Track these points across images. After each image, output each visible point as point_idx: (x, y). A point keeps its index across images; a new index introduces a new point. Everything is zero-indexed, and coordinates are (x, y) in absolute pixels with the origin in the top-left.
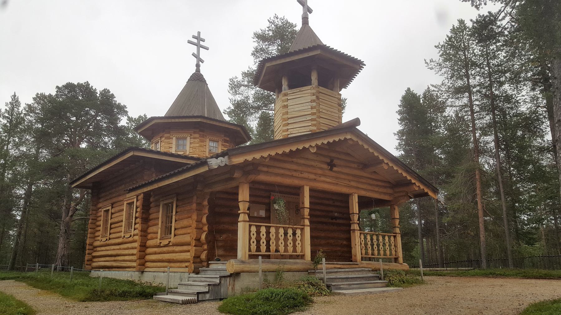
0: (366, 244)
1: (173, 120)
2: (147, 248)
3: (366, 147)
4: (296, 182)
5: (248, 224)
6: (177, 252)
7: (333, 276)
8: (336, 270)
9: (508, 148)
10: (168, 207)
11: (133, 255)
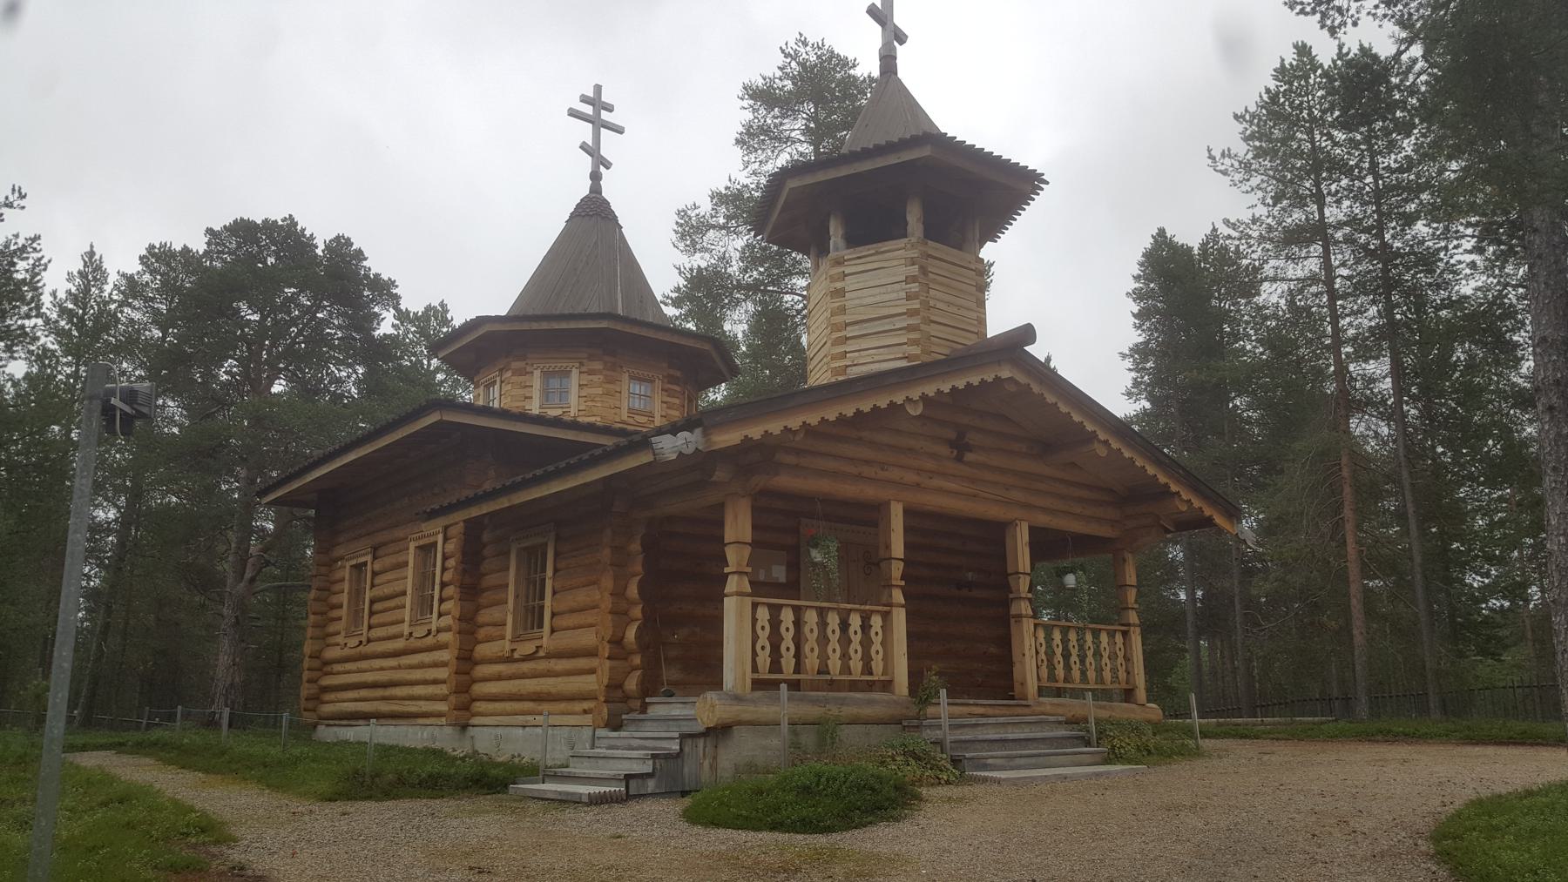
0: (1050, 654)
1: (535, 326)
2: (477, 664)
3: (1050, 399)
4: (869, 492)
5: (748, 600)
6: (557, 675)
7: (967, 735)
8: (973, 721)
9: (1428, 394)
10: (533, 560)
11: (435, 682)
